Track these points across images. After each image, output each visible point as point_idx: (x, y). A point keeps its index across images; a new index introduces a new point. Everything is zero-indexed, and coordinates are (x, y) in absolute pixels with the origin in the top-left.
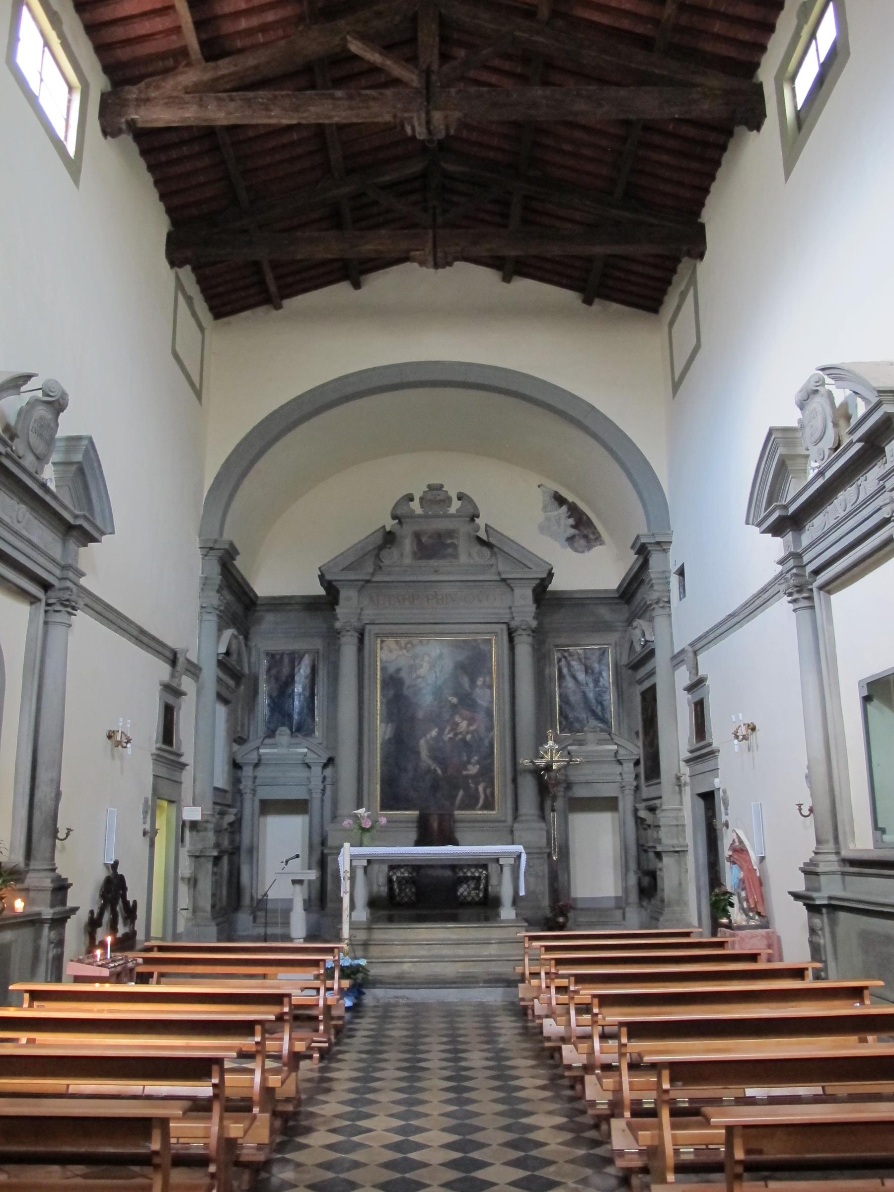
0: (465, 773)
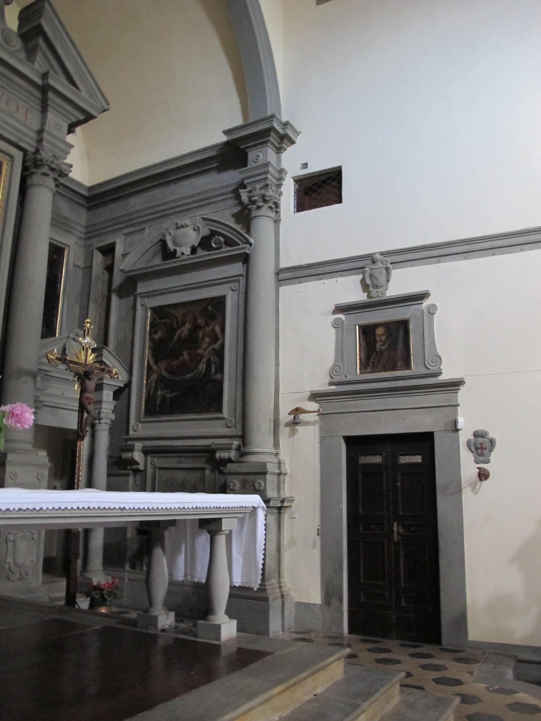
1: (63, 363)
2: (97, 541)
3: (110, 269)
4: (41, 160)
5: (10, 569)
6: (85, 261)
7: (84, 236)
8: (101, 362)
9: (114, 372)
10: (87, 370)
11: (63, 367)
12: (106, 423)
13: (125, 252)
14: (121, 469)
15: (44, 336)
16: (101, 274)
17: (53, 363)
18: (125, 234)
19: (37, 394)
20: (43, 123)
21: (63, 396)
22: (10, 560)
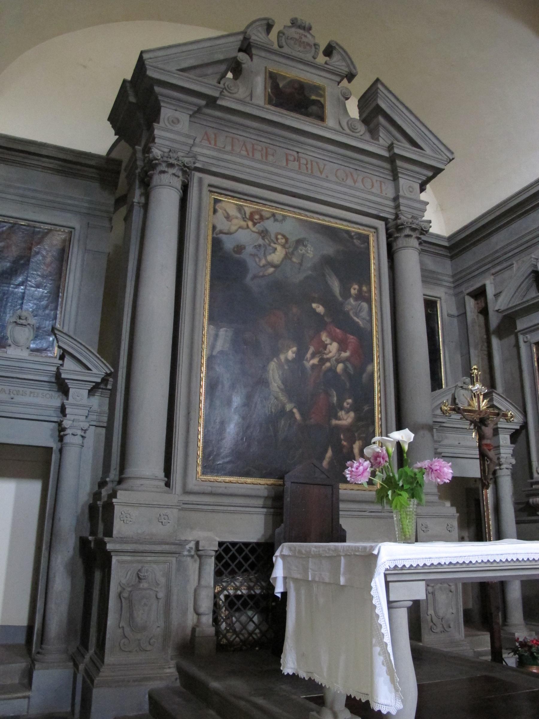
0: (334, 422)
1: (458, 413)
2: (515, 594)
3: (484, 312)
4: (402, 224)
5: (432, 622)
6: (458, 309)
7: (452, 285)
8: (493, 406)
9: (509, 415)
10: (482, 416)
11: (456, 416)
12: (507, 469)
13: (498, 291)
14: (529, 515)
15: (433, 389)
16: (476, 318)
17: (447, 414)
18: (493, 274)
19: (436, 446)
20: (397, 189)
21: (459, 446)
22: (431, 612)
